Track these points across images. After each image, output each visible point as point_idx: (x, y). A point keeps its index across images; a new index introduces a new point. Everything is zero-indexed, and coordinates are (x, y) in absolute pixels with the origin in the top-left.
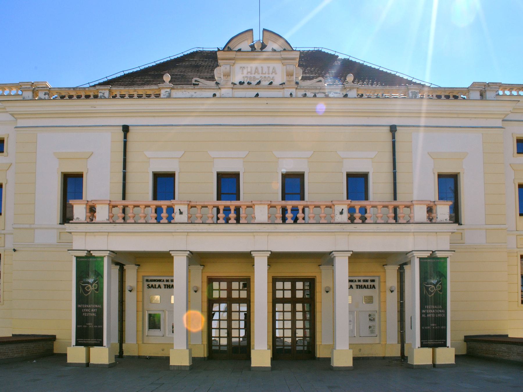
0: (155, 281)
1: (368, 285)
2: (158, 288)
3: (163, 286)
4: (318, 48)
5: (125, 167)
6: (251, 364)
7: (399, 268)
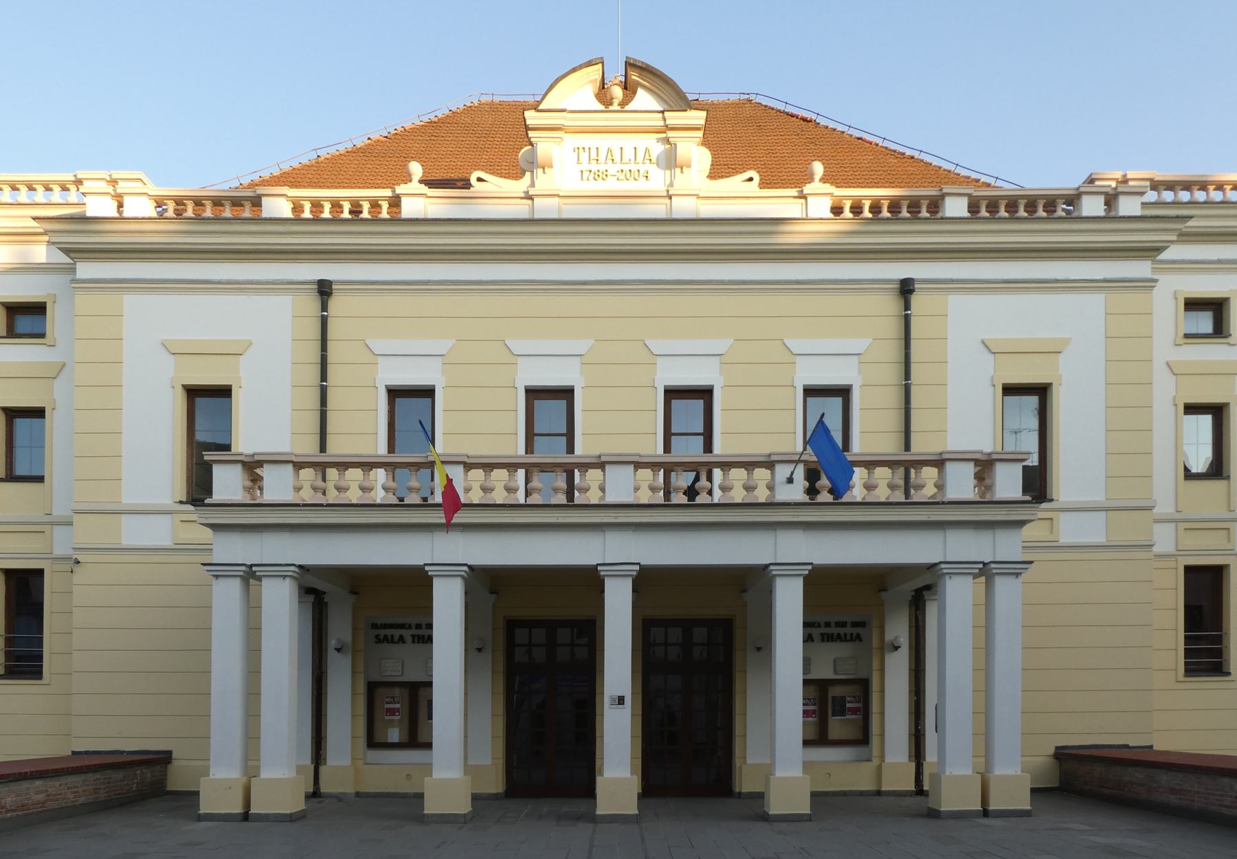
0: (391, 626)
1: (845, 634)
2: (398, 642)
3: (409, 639)
4: (748, 94)
5: (324, 376)
6: (596, 807)
7: (912, 596)
